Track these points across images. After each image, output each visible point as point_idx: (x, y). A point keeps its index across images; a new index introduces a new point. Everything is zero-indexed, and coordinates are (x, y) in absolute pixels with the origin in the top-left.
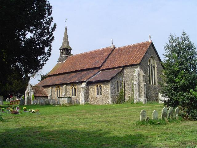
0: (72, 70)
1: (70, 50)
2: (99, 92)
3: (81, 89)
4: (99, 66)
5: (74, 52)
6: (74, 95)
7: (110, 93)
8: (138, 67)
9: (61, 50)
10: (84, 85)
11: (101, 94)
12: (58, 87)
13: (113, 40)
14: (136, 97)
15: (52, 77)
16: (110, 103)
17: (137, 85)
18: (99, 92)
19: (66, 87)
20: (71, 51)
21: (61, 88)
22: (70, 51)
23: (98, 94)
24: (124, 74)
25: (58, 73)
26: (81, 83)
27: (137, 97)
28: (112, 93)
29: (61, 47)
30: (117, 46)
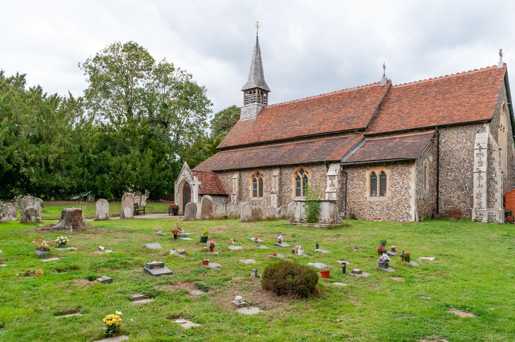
0: (284, 137)
1: (267, 92)
2: (378, 186)
3: (329, 182)
4: (362, 127)
5: (273, 100)
6: (302, 194)
7: (412, 191)
8: (484, 130)
9: (245, 91)
10: (334, 170)
11: (261, 195)
12: (258, 174)
13: (384, 67)
14: (480, 204)
15: (460, 130)
16: (413, 216)
17: (237, 180)
18: (378, 186)
19: (281, 174)
20: (267, 95)
21: (265, 175)
22: (265, 95)
23: (255, 195)
24: (440, 146)
25: (247, 142)
26: (328, 164)
27: (484, 204)
28: (417, 192)
29: (247, 84)
30: (399, 80)
